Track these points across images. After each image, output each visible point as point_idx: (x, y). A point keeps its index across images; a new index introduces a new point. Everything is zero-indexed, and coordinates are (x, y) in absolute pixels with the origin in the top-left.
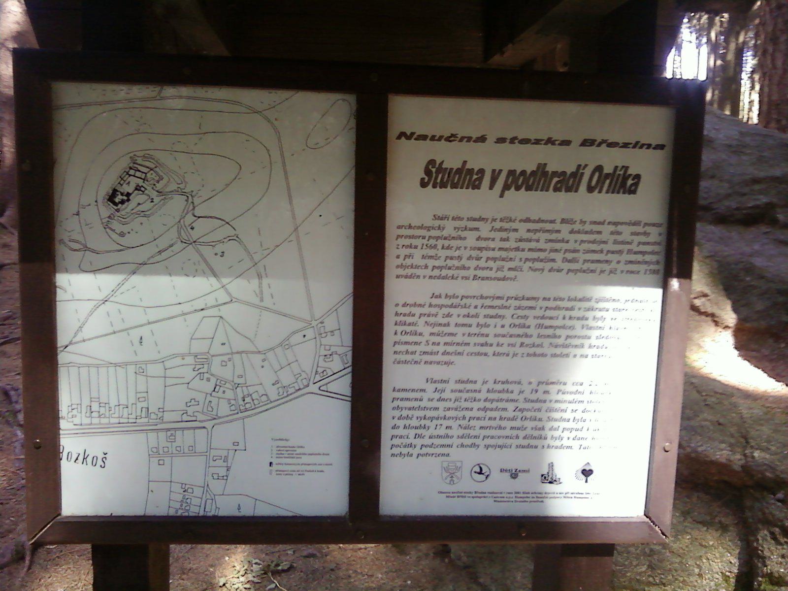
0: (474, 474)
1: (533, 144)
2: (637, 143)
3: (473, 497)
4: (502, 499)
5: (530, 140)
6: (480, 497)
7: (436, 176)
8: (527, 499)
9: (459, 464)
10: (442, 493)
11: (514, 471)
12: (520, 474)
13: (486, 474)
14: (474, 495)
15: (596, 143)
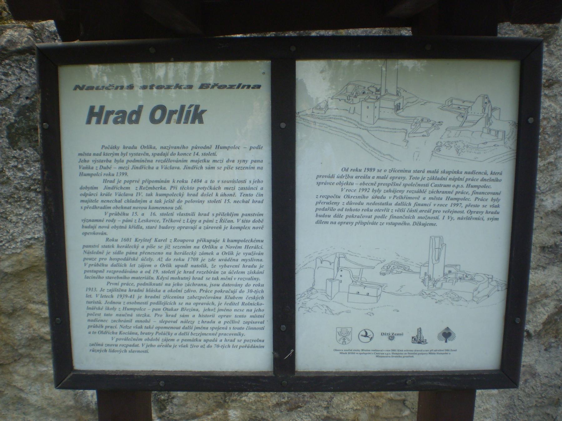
0: (361, 337)
1: (228, 88)
2: (240, 85)
3: (360, 354)
4: (382, 355)
5: (226, 86)
6: (366, 354)
7: (96, 115)
8: (401, 355)
9: (349, 330)
10: (336, 350)
11: (391, 335)
12: (396, 337)
13: (370, 337)
14: (361, 352)
15: (210, 86)
